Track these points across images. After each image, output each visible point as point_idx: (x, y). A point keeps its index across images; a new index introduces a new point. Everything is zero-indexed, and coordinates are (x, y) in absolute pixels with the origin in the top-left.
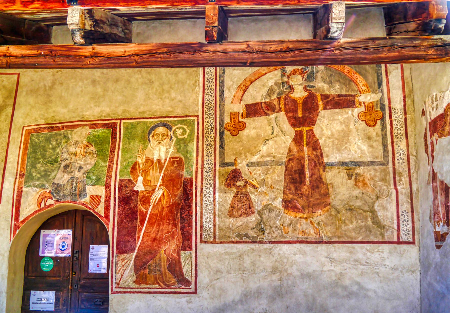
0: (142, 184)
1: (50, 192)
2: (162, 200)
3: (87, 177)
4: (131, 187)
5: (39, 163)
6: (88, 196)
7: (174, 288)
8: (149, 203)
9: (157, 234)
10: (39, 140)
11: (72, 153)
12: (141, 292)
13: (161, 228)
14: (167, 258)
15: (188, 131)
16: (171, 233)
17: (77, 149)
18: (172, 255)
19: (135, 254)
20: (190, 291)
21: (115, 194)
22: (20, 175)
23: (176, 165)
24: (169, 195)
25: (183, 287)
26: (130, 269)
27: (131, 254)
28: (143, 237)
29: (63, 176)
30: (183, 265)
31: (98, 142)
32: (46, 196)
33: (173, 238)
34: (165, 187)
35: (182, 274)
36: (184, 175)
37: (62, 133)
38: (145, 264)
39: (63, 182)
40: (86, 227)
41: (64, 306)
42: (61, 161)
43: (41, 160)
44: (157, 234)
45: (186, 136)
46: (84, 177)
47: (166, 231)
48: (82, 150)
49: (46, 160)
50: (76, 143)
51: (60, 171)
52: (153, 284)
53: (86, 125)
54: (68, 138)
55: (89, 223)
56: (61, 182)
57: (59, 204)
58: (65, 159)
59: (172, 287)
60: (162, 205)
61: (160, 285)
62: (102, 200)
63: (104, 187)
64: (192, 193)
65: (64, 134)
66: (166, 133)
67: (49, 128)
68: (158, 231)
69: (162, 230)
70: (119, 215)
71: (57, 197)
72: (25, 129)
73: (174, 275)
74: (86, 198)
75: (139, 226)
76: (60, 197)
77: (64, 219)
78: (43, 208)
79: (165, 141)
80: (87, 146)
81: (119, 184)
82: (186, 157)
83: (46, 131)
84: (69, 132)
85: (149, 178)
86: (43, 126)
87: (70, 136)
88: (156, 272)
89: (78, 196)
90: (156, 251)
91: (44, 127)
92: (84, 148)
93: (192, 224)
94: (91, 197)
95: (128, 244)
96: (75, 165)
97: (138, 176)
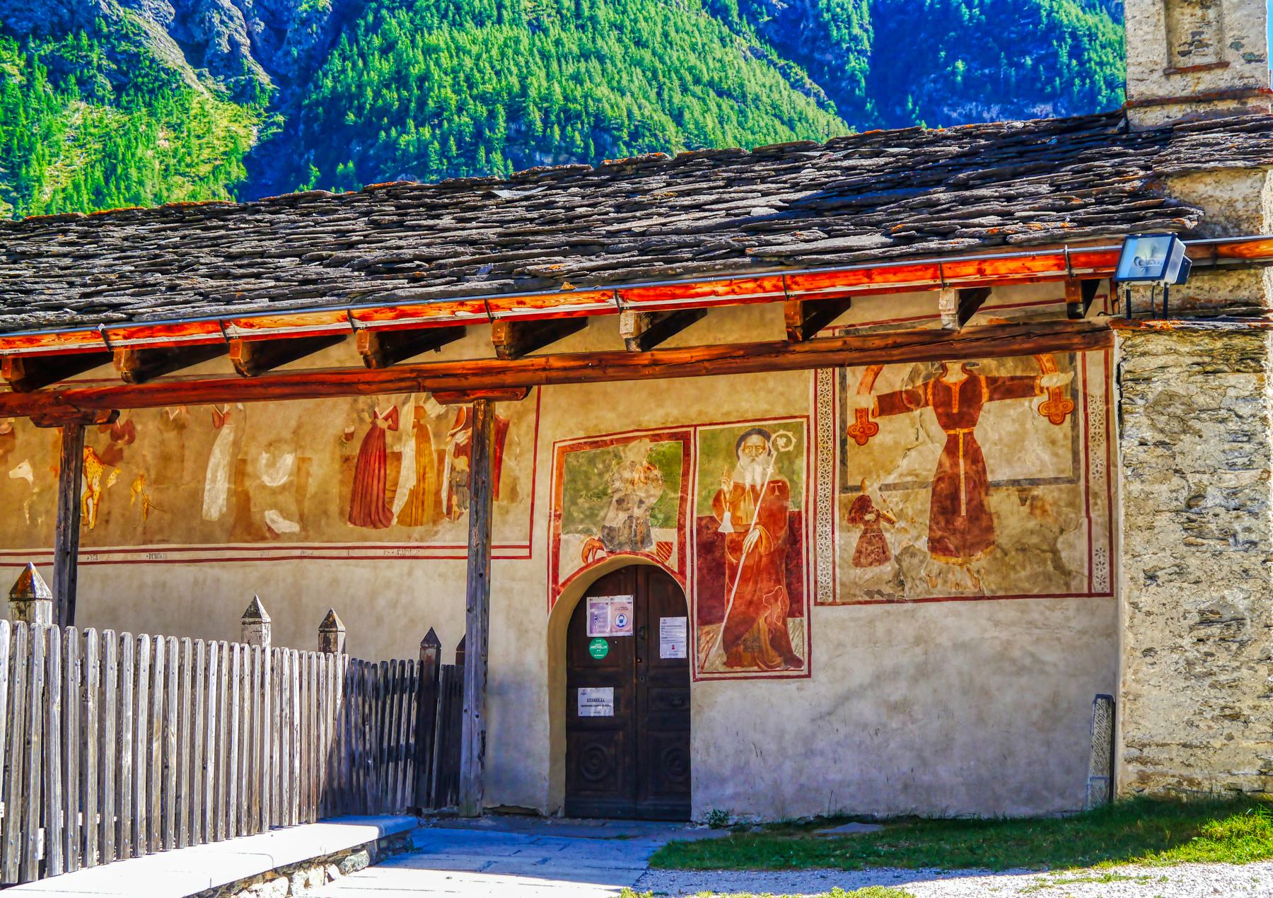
1: (599, 540)
8: (741, 550)
11: (627, 480)
15: (794, 440)
19: (724, 624)
23: (777, 493)
33: (776, 600)
35: (790, 651)
38: (738, 638)
43: (584, 493)
56: (614, 525)
57: (613, 557)
82: (791, 480)
83: (588, 449)
85: (739, 514)
90: (753, 620)
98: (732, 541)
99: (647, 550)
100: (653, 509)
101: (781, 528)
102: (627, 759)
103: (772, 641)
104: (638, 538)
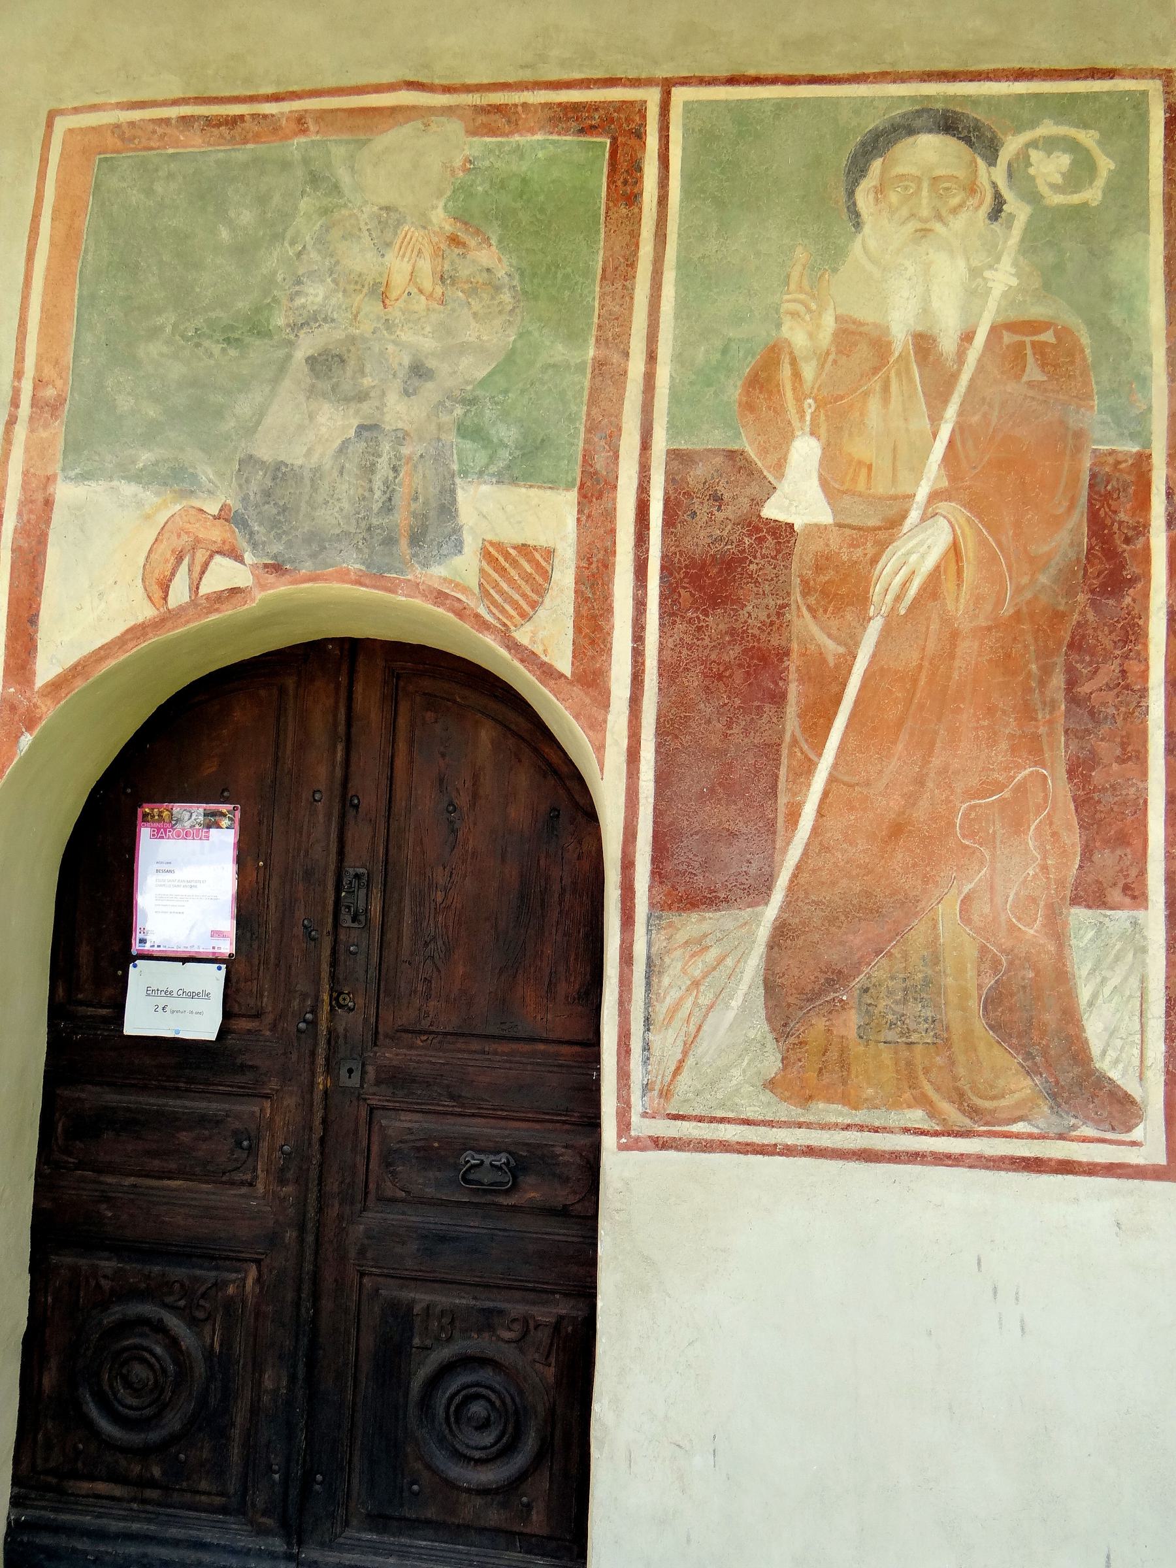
0: (815, 482)
1: (224, 515)
2: (948, 586)
3: (463, 431)
4: (745, 502)
5: (154, 333)
6: (471, 545)
7: (1031, 1136)
8: (862, 600)
9: (912, 800)
10: (149, 192)
11: (358, 281)
12: (810, 1151)
13: (936, 762)
14: (983, 950)
15: (1105, 165)
16: (1006, 793)
17: (390, 257)
18: (1012, 928)
19: (771, 911)
20: (1133, 1157)
21: (641, 538)
22: (35, 401)
23: (1033, 372)
24: (994, 558)
25: (1088, 1131)
26: (743, 1008)
27: (746, 913)
28: (820, 813)
29: (311, 417)
30: (1084, 994)
31: (524, 217)
32: (197, 540)
33: (1017, 825)
34: (970, 505)
35: (1078, 1053)
36: (1097, 435)
37: (297, 156)
38: (836, 978)
39: (309, 453)
40: (411, 742)
41: (282, 1182)
42: (295, 327)
43: (167, 319)
44: (912, 800)
45: (1092, 195)
46: (440, 427)
47: (974, 782)
48: (425, 265)
49: (199, 321)
50: (382, 225)
51: (287, 383)
52: (895, 1104)
53: (449, 110)
54: (336, 189)
55: (429, 716)
56: (295, 456)
57: (281, 589)
58: (313, 319)
59: (1015, 1128)
60: (946, 621)
61: (933, 1113)
62: (556, 576)
63: (573, 496)
64: (1147, 548)
65: (306, 161)
66: (961, 174)
67: (212, 123)
68: (920, 781)
69: (944, 771)
70: (668, 672)
71: (277, 548)
72: (62, 124)
73: (1029, 1056)
74: (458, 561)
75: (795, 742)
76: (290, 545)
77: (282, 691)
78: (182, 608)
79: (959, 223)
80: (454, 240)
81: (671, 479)
82: (1101, 327)
83: (194, 142)
84: (339, 152)
85: (860, 449)
86: (173, 112)
87: (343, 176)
88: (907, 1033)
89: (404, 543)
90: (909, 905)
91: (183, 119)
92: (438, 253)
93: (1145, 741)
94: (486, 555)
95: (723, 850)
96: (382, 353)
97: (787, 437)
98: (822, 563)
99: (438, 573)
100: (470, 401)
101: (1056, 522)
102: (204, 1485)
103: (993, 1001)
104: (401, 518)
